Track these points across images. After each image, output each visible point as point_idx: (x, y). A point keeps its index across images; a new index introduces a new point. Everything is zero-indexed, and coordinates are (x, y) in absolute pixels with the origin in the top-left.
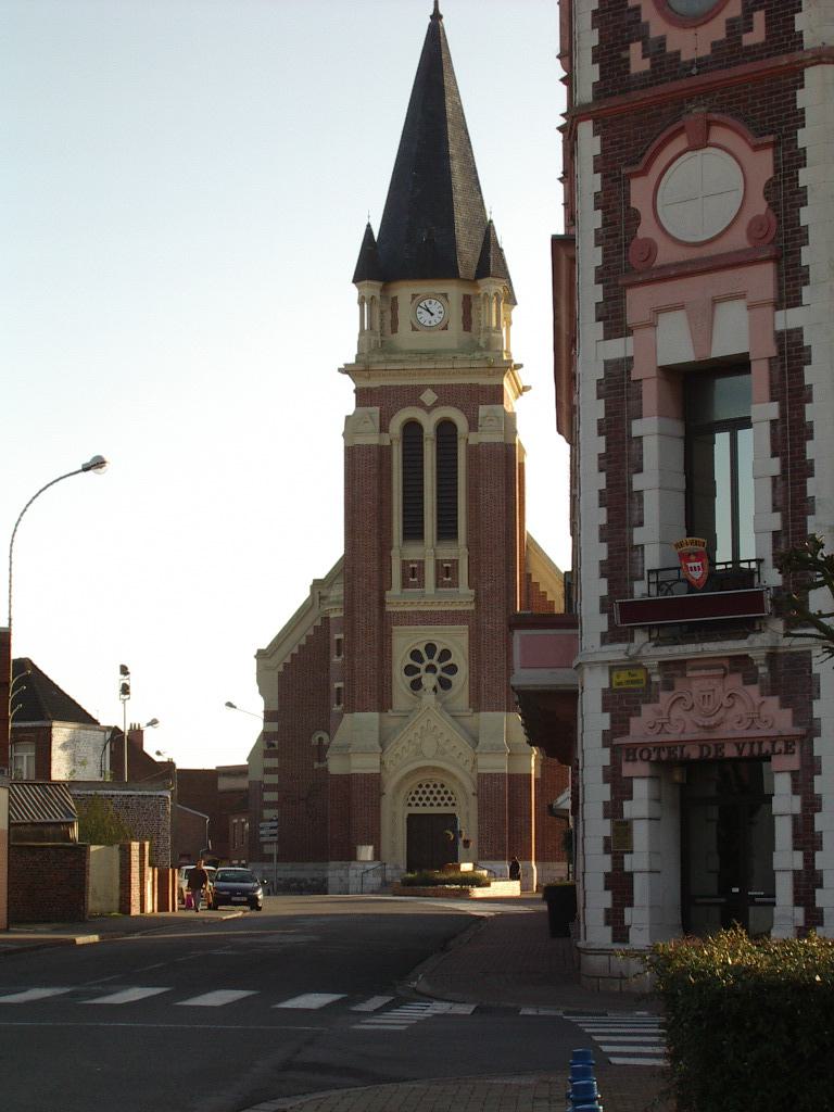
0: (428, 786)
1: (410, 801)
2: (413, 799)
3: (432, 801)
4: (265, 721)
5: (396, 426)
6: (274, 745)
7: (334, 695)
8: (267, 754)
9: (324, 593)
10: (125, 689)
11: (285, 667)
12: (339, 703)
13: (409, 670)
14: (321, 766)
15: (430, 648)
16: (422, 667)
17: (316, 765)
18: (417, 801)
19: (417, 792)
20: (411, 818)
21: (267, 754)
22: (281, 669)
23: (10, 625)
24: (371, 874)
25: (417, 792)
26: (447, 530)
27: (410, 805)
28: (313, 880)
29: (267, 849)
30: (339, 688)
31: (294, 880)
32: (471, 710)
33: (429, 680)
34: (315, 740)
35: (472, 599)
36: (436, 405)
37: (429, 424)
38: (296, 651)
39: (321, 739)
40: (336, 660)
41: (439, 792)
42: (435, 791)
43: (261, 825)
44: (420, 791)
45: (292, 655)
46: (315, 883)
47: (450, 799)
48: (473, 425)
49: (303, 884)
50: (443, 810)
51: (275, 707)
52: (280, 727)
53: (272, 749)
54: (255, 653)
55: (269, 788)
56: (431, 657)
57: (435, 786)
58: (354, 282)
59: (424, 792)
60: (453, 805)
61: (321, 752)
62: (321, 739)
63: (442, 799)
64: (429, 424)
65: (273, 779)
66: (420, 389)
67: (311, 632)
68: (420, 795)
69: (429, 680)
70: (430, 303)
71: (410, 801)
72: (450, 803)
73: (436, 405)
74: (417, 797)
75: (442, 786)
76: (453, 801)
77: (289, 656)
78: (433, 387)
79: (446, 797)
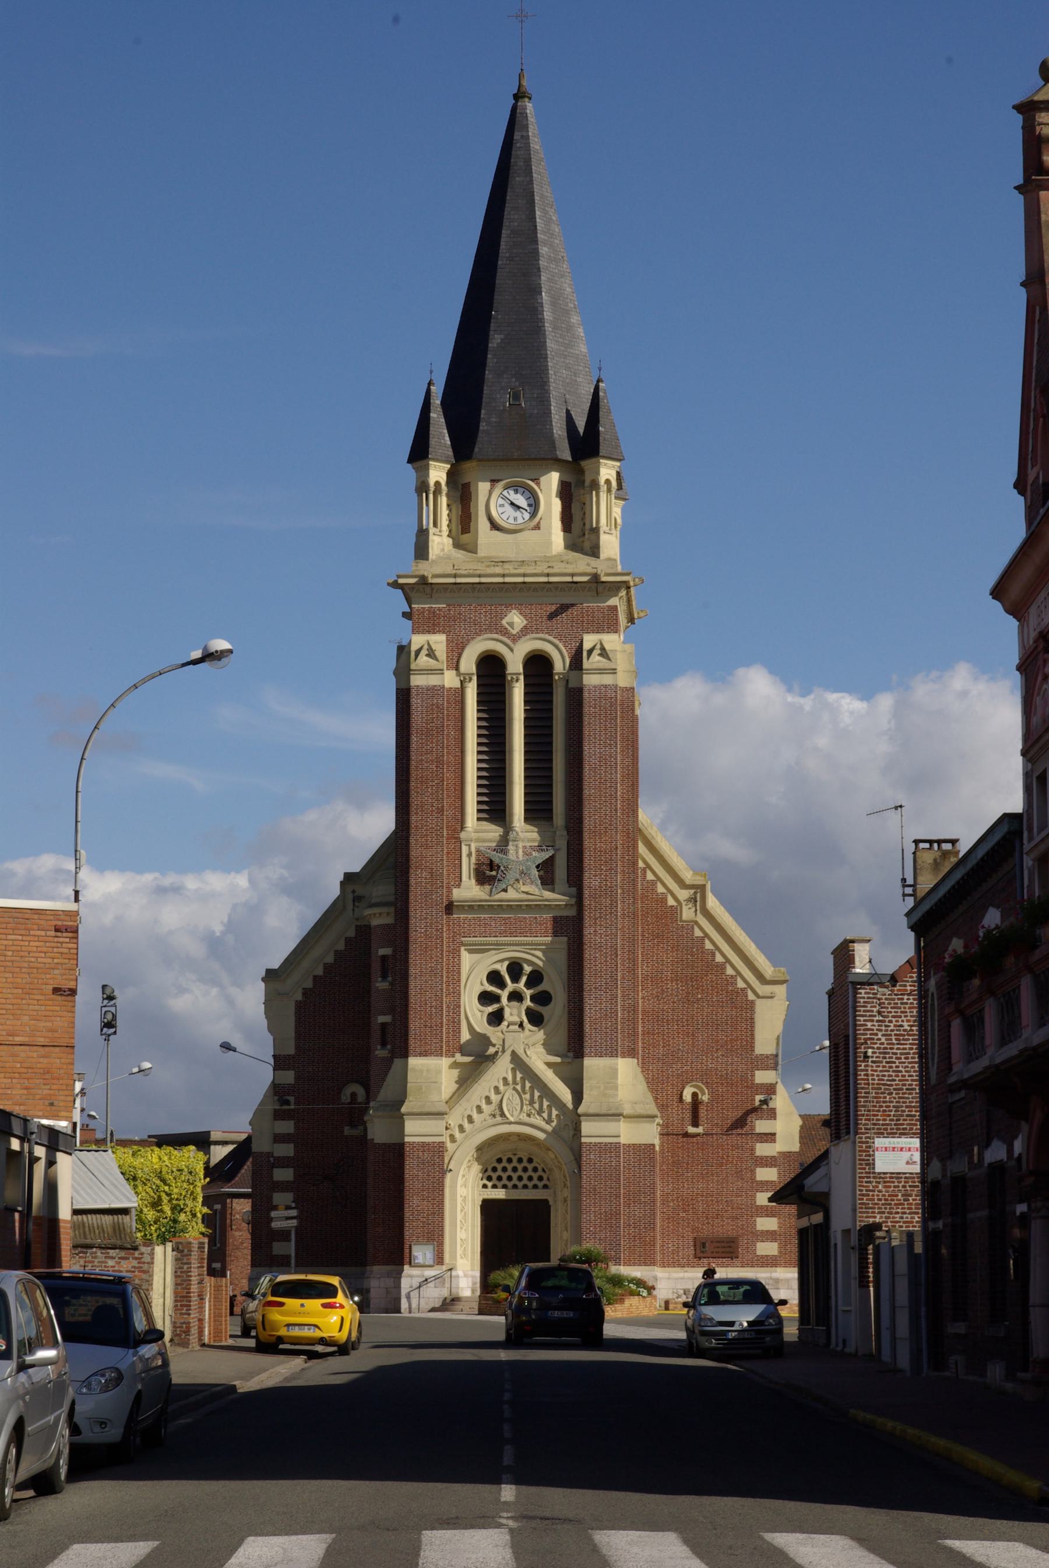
3: (515, 1181)
4: (275, 1069)
5: (469, 663)
6: (288, 1103)
7: (376, 1035)
8: (278, 1115)
9: (360, 891)
10: (109, 1024)
11: (304, 994)
14: (355, 1132)
15: (515, 969)
16: (504, 995)
17: (347, 1131)
20: (488, 1207)
21: (278, 1115)
22: (299, 996)
23: (76, 986)
30: (382, 1024)
32: (571, 1054)
34: (346, 1096)
36: (525, 631)
37: (515, 664)
38: (319, 971)
39: (354, 1095)
41: (525, 1169)
42: (520, 1167)
43: (273, 1214)
44: (499, 1167)
45: (315, 977)
51: (291, 1050)
52: (297, 1078)
53: (286, 1107)
54: (263, 974)
55: (283, 1162)
58: (408, 462)
60: (545, 1187)
61: (356, 1115)
62: (354, 1095)
63: (520, 1178)
64: (515, 664)
65: (286, 1150)
68: (510, 1173)
70: (515, 519)
72: (540, 1184)
73: (525, 631)
75: (530, 1161)
76: (545, 1182)
77: (311, 979)
79: (535, 1176)
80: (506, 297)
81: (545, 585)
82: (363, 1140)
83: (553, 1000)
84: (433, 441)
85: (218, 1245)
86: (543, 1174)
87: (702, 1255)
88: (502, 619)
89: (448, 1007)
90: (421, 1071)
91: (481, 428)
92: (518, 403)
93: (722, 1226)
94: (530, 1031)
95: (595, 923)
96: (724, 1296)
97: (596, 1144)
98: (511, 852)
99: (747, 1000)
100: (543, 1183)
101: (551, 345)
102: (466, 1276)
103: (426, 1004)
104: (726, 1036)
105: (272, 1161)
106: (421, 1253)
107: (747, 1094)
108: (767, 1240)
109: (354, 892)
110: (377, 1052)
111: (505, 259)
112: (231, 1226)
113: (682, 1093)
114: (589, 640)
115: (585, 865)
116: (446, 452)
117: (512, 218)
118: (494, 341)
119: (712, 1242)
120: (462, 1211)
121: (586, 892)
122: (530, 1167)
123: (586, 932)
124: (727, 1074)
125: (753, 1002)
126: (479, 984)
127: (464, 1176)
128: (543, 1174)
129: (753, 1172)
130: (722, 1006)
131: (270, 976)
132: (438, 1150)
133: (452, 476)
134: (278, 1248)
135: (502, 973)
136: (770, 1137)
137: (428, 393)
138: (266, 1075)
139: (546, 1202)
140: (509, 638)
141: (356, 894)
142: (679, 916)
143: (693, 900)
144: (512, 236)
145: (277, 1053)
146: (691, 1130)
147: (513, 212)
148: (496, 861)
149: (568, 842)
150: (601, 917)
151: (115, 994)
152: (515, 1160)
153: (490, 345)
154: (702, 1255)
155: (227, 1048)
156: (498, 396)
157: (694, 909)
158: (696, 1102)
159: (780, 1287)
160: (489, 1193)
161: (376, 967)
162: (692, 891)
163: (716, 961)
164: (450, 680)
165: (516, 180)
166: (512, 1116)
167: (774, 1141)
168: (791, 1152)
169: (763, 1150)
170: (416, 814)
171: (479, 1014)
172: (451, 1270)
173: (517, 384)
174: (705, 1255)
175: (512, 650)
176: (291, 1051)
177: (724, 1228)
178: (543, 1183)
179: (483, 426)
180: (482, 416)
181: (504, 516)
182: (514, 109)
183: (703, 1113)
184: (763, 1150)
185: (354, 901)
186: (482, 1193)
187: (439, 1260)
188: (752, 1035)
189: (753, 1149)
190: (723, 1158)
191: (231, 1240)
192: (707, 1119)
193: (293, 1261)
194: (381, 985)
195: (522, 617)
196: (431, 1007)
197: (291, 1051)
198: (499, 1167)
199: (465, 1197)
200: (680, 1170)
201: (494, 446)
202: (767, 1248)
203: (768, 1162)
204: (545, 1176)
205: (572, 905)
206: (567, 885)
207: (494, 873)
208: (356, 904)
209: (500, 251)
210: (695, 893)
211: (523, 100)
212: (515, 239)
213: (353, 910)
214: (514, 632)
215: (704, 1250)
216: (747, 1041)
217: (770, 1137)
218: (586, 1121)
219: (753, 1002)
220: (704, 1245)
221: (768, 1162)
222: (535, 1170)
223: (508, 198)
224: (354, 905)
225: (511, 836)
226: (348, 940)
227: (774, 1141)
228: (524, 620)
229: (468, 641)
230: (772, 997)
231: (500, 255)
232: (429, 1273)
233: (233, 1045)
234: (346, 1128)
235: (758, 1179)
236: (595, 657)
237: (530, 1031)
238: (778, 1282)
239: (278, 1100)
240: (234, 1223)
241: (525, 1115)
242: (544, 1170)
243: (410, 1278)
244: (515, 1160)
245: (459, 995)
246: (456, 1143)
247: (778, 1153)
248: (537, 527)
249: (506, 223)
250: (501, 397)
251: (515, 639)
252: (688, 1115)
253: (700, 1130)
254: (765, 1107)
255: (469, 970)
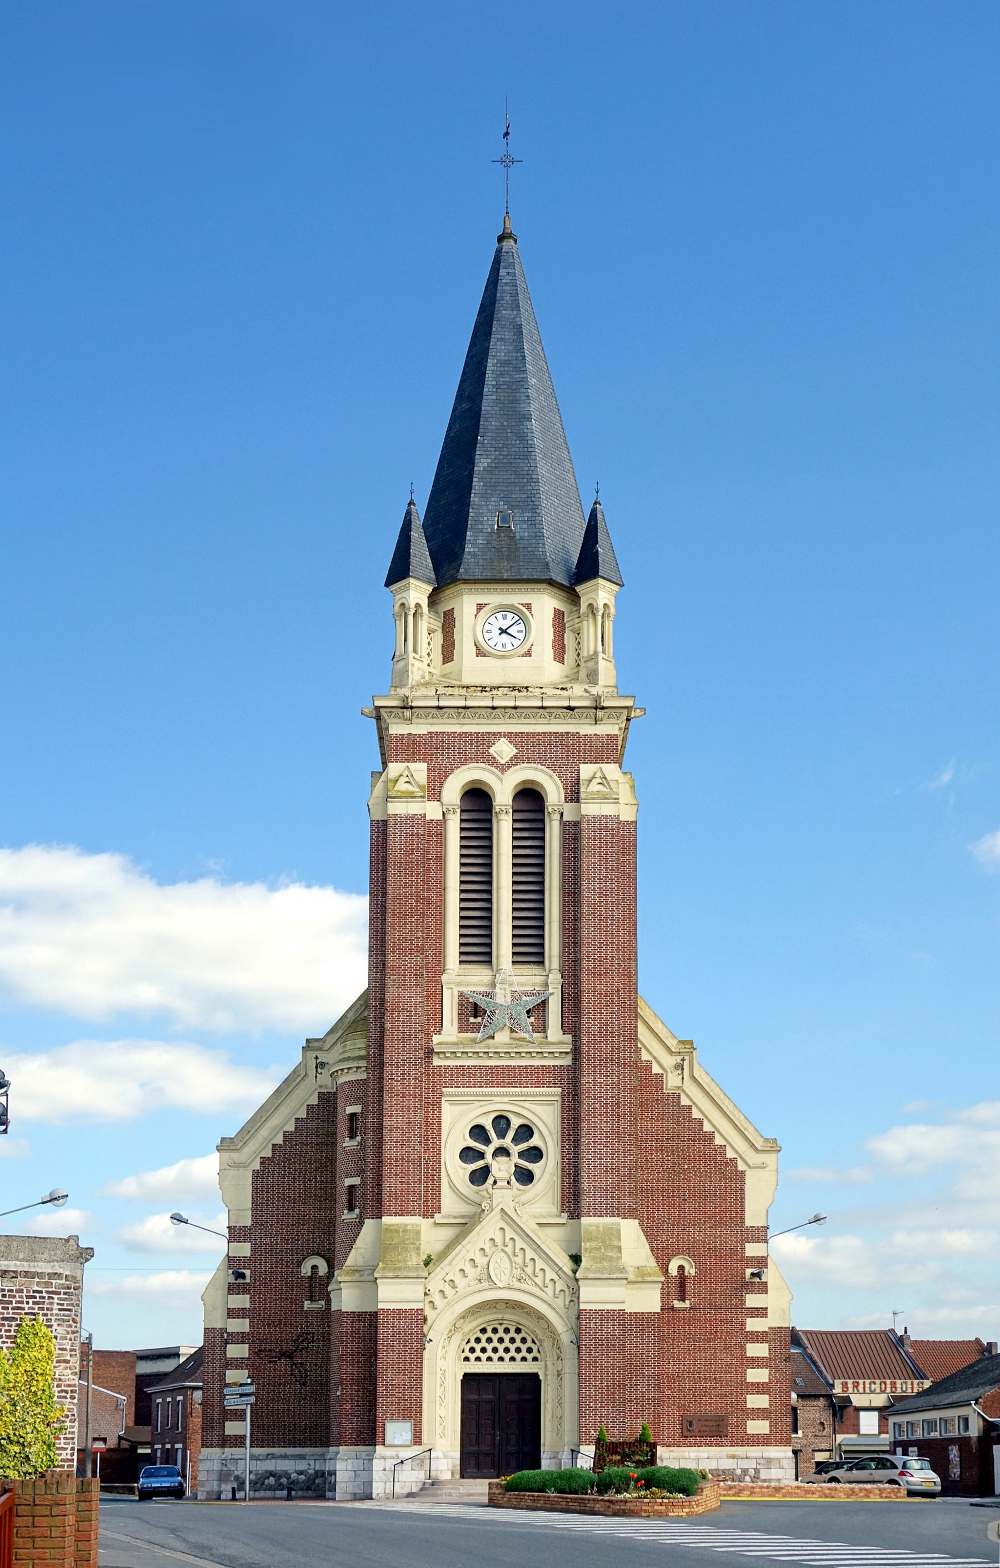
0: (495, 1331)
1: (467, 1353)
2: (472, 1350)
3: (501, 1353)
6: (242, 1276)
7: (342, 1199)
8: (232, 1289)
12: (351, 1209)
13: (468, 1154)
15: (501, 1122)
16: (489, 1150)
18: (478, 1353)
19: (478, 1340)
20: (469, 1381)
21: (232, 1289)
22: (257, 1166)
24: (407, 1465)
25: (478, 1340)
26: (13, 1313)
27: (467, 1359)
28: (300, 1473)
29: (232, 1428)
31: (271, 1474)
32: (565, 1215)
33: (502, 1169)
34: (306, 1270)
35: (568, 1049)
36: (515, 761)
37: (503, 795)
40: (348, 1143)
41: (512, 1340)
46: (302, 1477)
47: (529, 1350)
48: (574, 795)
49: (284, 1481)
50: (518, 1368)
52: (254, 1250)
53: (240, 1281)
55: (239, 1338)
56: (502, 1134)
57: (507, 1331)
59: (489, 1340)
60: (535, 1359)
63: (518, 1350)
64: (503, 795)
66: (485, 740)
67: (303, 1114)
68: (495, 1343)
69: (502, 1169)
71: (467, 1353)
72: (529, 1357)
73: (515, 761)
74: (478, 1347)
76: (535, 1354)
77: (293, 1121)
78: (510, 736)
80: (493, 423)
81: (538, 710)
82: (326, 1315)
83: (544, 1157)
84: (413, 560)
85: (180, 1429)
86: (532, 1345)
87: (688, 1434)
88: (489, 747)
89: (427, 1163)
90: (397, 1232)
91: (466, 550)
92: (508, 526)
93: (710, 1403)
94: (518, 1189)
95: (595, 1072)
96: (712, 1474)
97: (596, 1312)
98: (498, 996)
99: (736, 1171)
100: (532, 1355)
101: (543, 470)
102: (445, 1457)
103: (402, 1158)
104: (715, 1208)
105: (226, 1337)
106: (397, 1432)
107: (737, 1267)
108: (758, 1418)
109: (317, 1058)
110: (343, 1217)
111: (491, 387)
112: (191, 1414)
113: (667, 1266)
114: (586, 770)
115: (583, 1008)
116: (428, 574)
117: (498, 349)
118: (480, 464)
119: (699, 1420)
120: (441, 1385)
121: (585, 1039)
122: (518, 1338)
123: (584, 1080)
124: (715, 1247)
125: (743, 1173)
126: (462, 1138)
127: (444, 1347)
128: (532, 1345)
129: (743, 1348)
130: (710, 1177)
131: (226, 1145)
132: (419, 1318)
133: (433, 599)
134: (232, 1428)
135: (487, 1128)
136: (761, 1312)
137: (408, 514)
138: (220, 1247)
139: (536, 1376)
140: (497, 767)
141: (318, 1061)
142: (664, 1084)
143: (680, 1067)
144: (499, 365)
145: (232, 1225)
146: (677, 1304)
147: (499, 343)
148: (482, 1005)
149: (562, 986)
150: (600, 1065)
151: (6, 1078)
152: (501, 1329)
153: (476, 468)
154: (688, 1434)
155: (178, 1220)
156: (485, 519)
157: (681, 1076)
158: (682, 1277)
159: (772, 1467)
160: (472, 1367)
161: (342, 1126)
162: (679, 1058)
163: (704, 1131)
164: (433, 811)
165: (503, 312)
166: (500, 1281)
167: (766, 1316)
168: (782, 1328)
169: (753, 1324)
170: (393, 952)
171: (461, 1172)
172: (430, 1450)
173: (506, 507)
174: (693, 1434)
175: (501, 780)
176: (248, 1222)
177: (711, 1406)
178: (532, 1355)
179: (468, 548)
180: (468, 538)
181: (492, 643)
182: (499, 251)
183: (689, 1287)
184: (753, 1324)
185: (316, 1067)
186: (463, 1366)
187: (417, 1440)
188: (743, 1207)
189: (743, 1324)
190: (711, 1333)
191: (191, 1426)
192: (694, 1293)
193: (248, 1442)
194: (348, 1143)
195: (512, 746)
196: (408, 1162)
197: (248, 1222)
198: (484, 1338)
199: (445, 1371)
200: (665, 1346)
201: (481, 567)
202: (758, 1427)
203: (758, 1337)
204: (535, 1348)
205: (567, 1053)
206: (562, 1032)
207: (479, 1019)
208: (319, 1070)
209: (486, 379)
210: (683, 1060)
211: (509, 240)
212: (502, 369)
213: (316, 1077)
214: (503, 762)
215: (692, 1429)
216: (737, 1212)
217: (761, 1312)
218: (586, 1285)
219: (743, 1173)
220: (691, 1424)
221: (758, 1337)
222: (524, 1340)
223: (494, 329)
224: (317, 1071)
225: (499, 978)
226: (310, 1108)
227: (766, 1316)
228: (514, 748)
229: (452, 770)
230: (764, 1168)
231: (486, 383)
232: (406, 1453)
233: (185, 1216)
234: (306, 1303)
235: (748, 1355)
236: (594, 787)
237: (518, 1189)
238: (771, 1462)
239: (233, 1273)
240: (193, 1411)
241: (515, 1280)
242: (533, 1342)
243: (383, 1457)
244: (501, 1329)
245: (440, 1150)
246: (436, 1311)
247: (769, 1328)
248: (528, 654)
249: (491, 353)
250: (488, 520)
251: (504, 768)
252: (674, 1290)
253: (687, 1304)
254: (757, 1280)
255: (450, 1125)
